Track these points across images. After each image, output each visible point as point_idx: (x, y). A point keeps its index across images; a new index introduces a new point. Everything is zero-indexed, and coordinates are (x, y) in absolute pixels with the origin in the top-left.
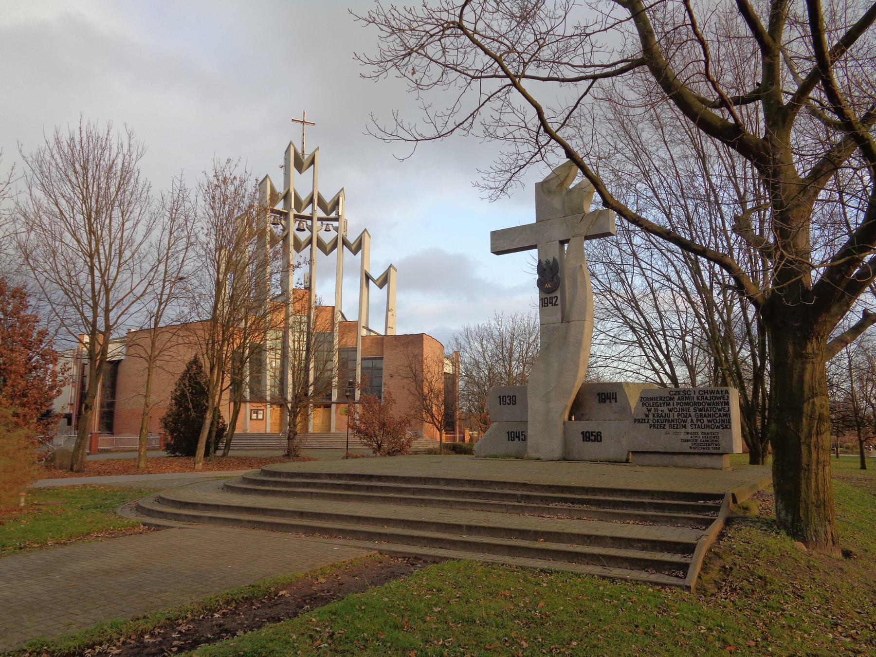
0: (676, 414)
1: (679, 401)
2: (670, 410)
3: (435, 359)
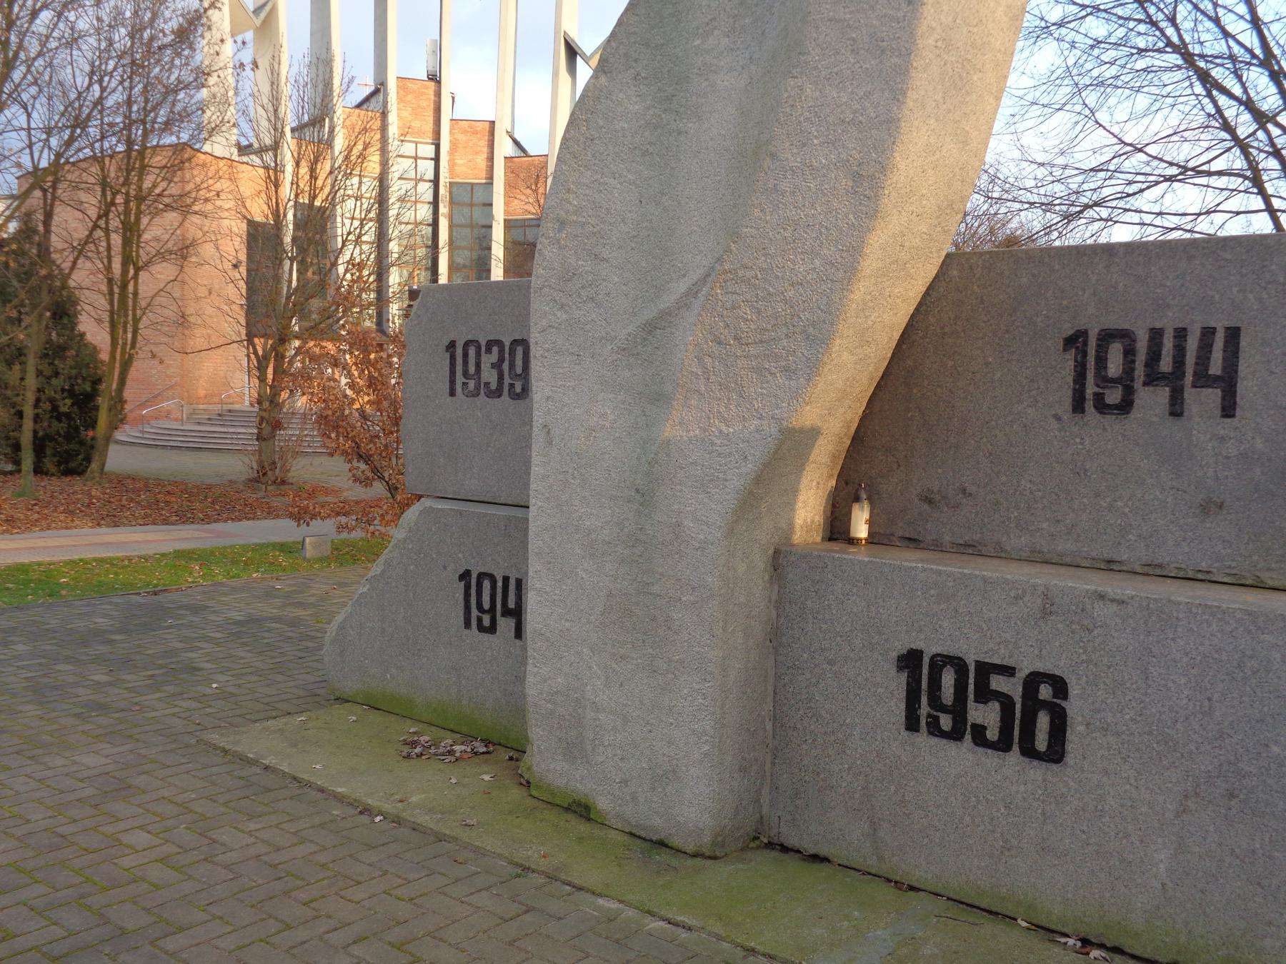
3: (865, 258)
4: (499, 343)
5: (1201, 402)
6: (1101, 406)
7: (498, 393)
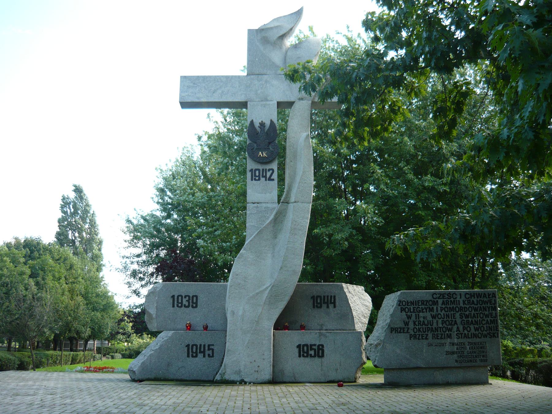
0: (440, 321)
1: (443, 306)
2: (433, 317)
4: (189, 296)
5: (331, 306)
6: (317, 307)
7: (188, 306)
